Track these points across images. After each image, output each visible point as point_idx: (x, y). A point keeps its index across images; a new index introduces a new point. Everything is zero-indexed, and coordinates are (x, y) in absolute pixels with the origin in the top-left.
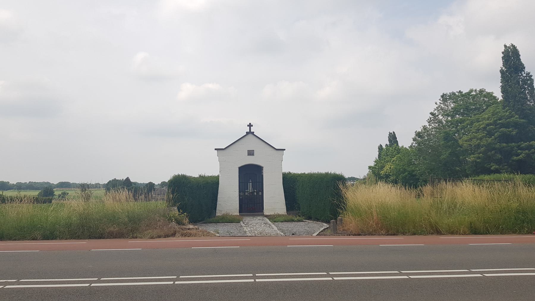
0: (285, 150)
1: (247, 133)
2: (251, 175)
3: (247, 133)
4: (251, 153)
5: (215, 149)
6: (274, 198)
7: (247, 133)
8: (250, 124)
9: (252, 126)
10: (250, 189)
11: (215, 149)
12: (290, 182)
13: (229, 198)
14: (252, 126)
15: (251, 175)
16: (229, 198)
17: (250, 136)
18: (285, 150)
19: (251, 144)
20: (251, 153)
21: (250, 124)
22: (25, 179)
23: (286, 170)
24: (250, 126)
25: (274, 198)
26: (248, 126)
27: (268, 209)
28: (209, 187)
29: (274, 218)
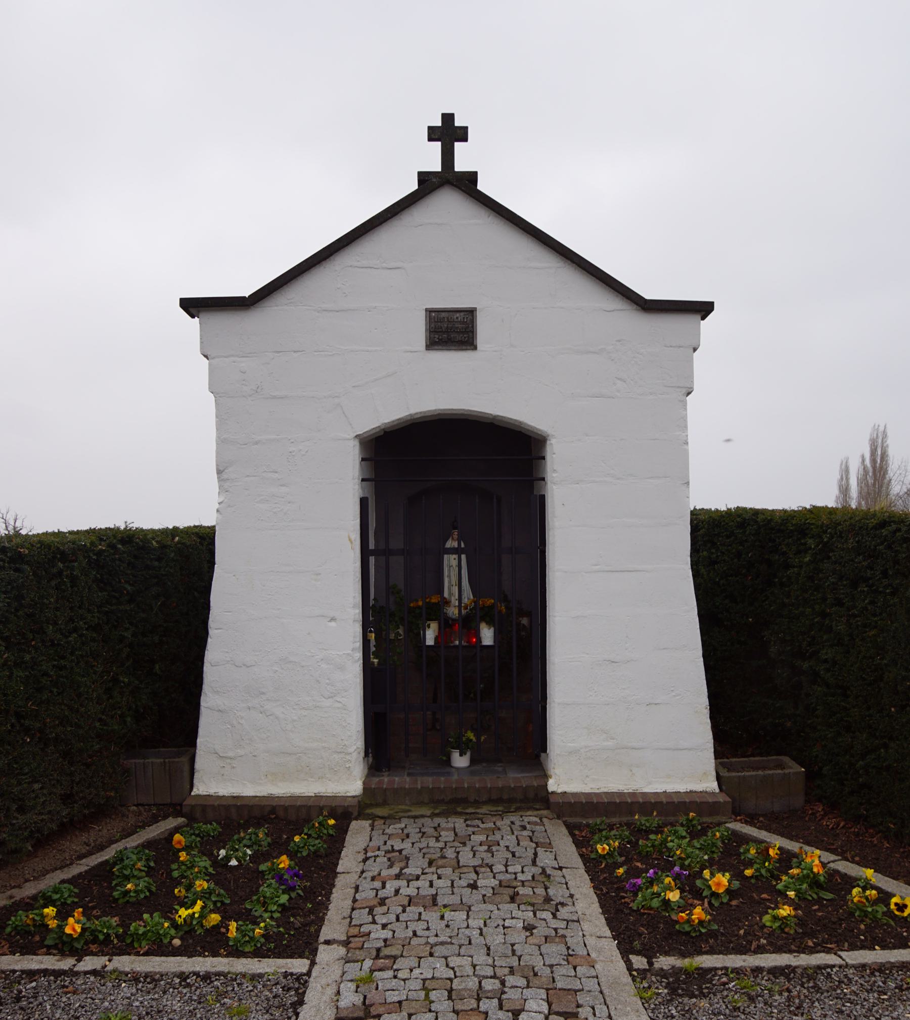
0: (704, 309)
1: (423, 177)
2: (454, 504)
3: (428, 184)
4: (452, 330)
5: (192, 306)
6: (628, 693)
7: (423, 177)
8: (448, 118)
9: (462, 135)
10: (456, 582)
11: (192, 306)
12: (747, 567)
13: (285, 694)
14: (462, 135)
15: (454, 504)
16: (285, 694)
17: (447, 204)
18: (704, 309)
19: (449, 259)
20: (452, 330)
21: (448, 118)
22: (359, 644)
23: (718, 493)
24: (448, 133)
25: (628, 693)
26: (433, 134)
27: (577, 764)
28: (141, 599)
29: (626, 840)
